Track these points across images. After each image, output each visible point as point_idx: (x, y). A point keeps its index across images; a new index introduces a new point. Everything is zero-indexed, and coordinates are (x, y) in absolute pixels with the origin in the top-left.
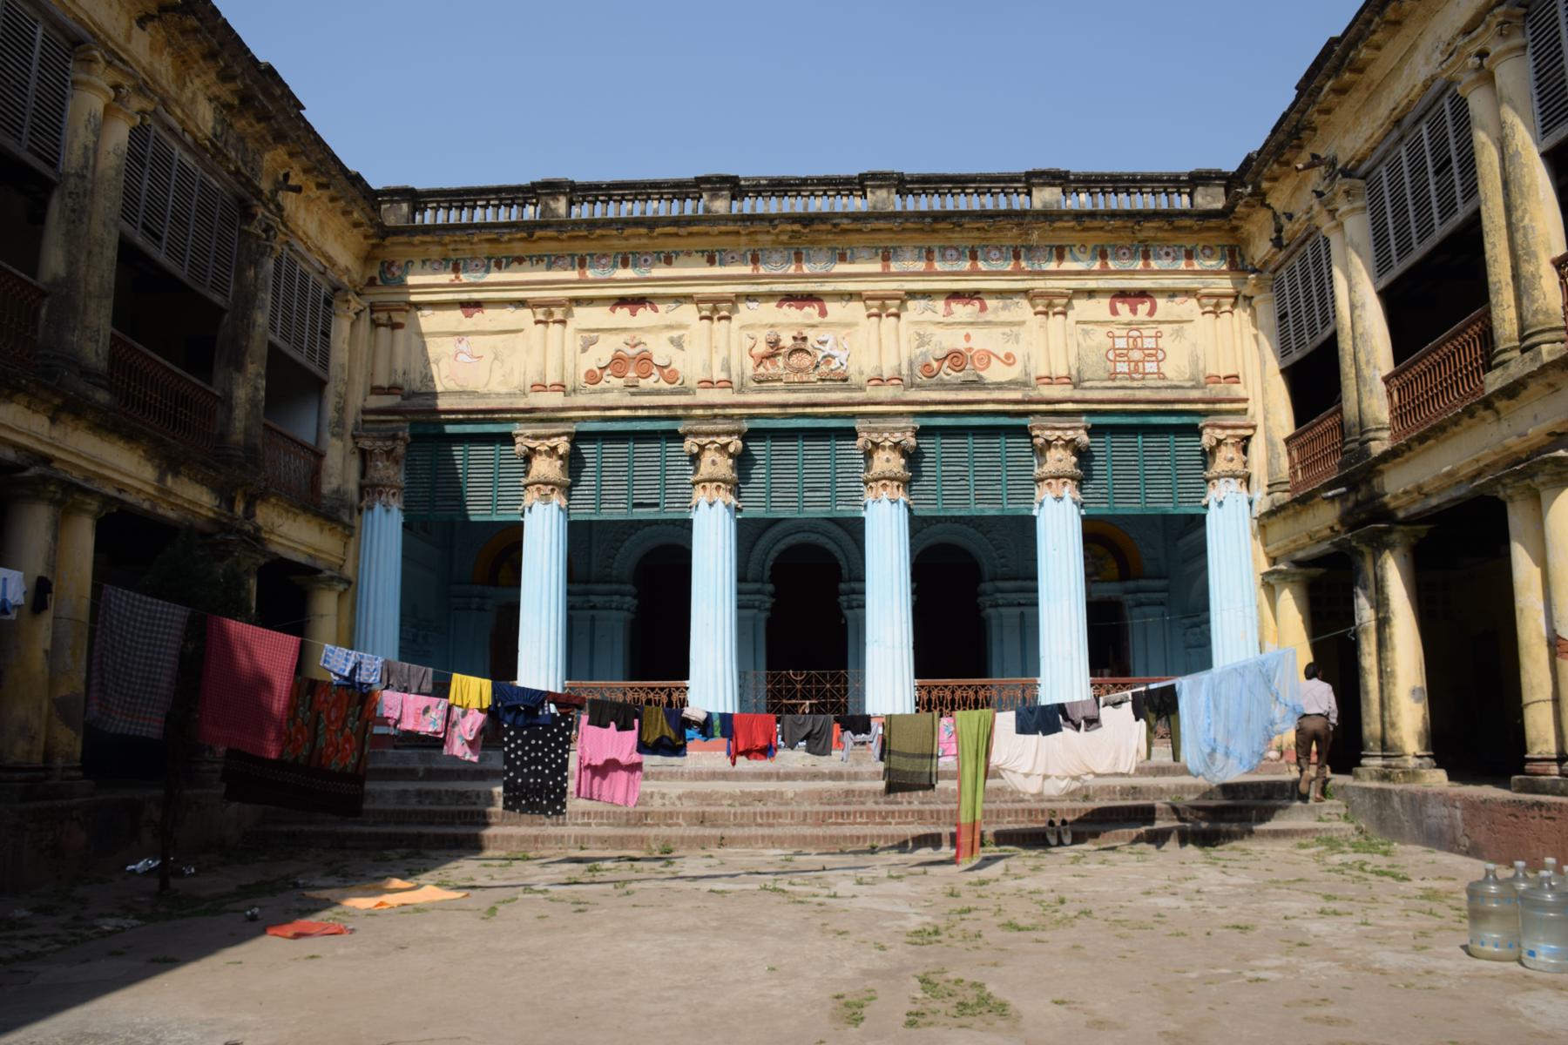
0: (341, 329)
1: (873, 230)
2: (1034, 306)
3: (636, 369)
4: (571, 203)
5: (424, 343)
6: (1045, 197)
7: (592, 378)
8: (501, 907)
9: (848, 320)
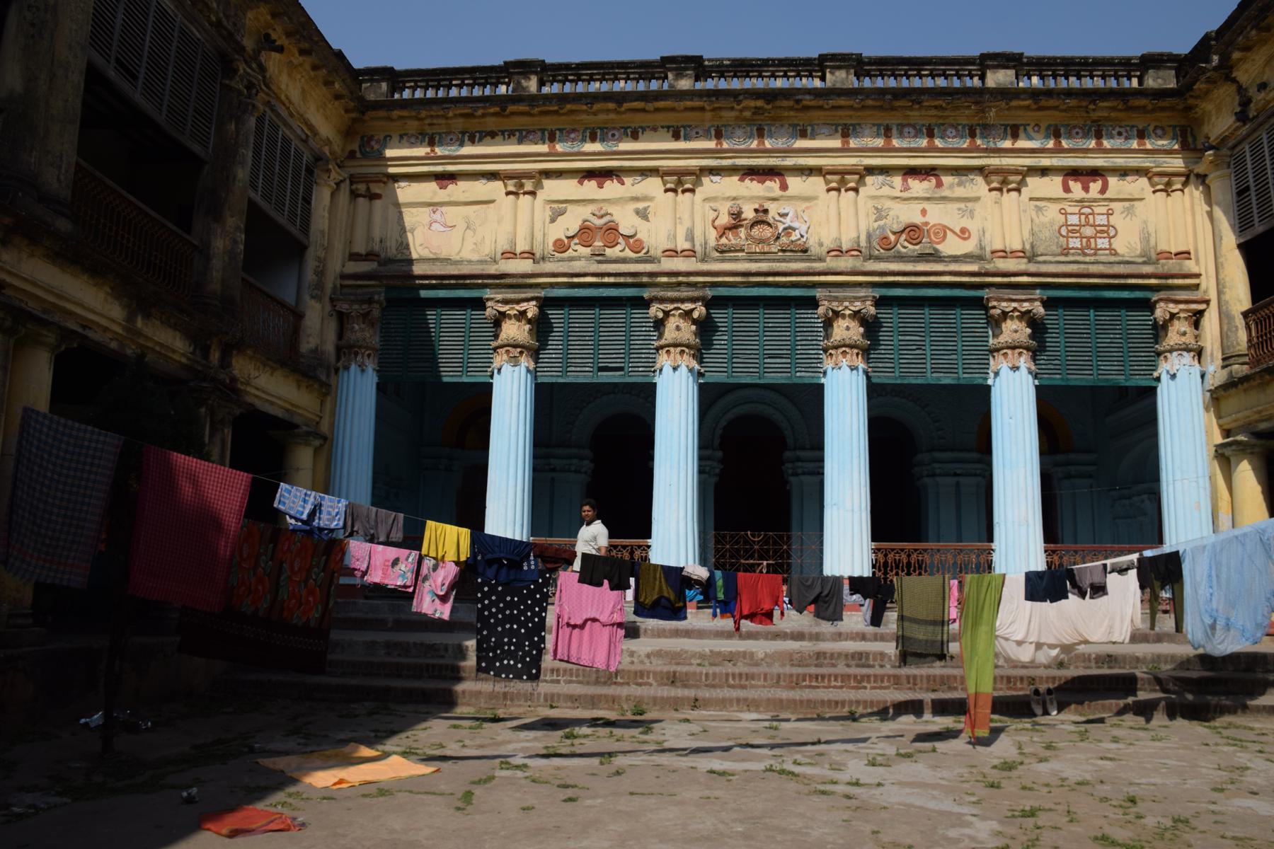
0: (322, 197)
1: (834, 107)
2: (988, 183)
3: (602, 239)
4: (542, 83)
5: (401, 213)
6: (999, 78)
7: (561, 246)
8: (478, 791)
9: (809, 193)
